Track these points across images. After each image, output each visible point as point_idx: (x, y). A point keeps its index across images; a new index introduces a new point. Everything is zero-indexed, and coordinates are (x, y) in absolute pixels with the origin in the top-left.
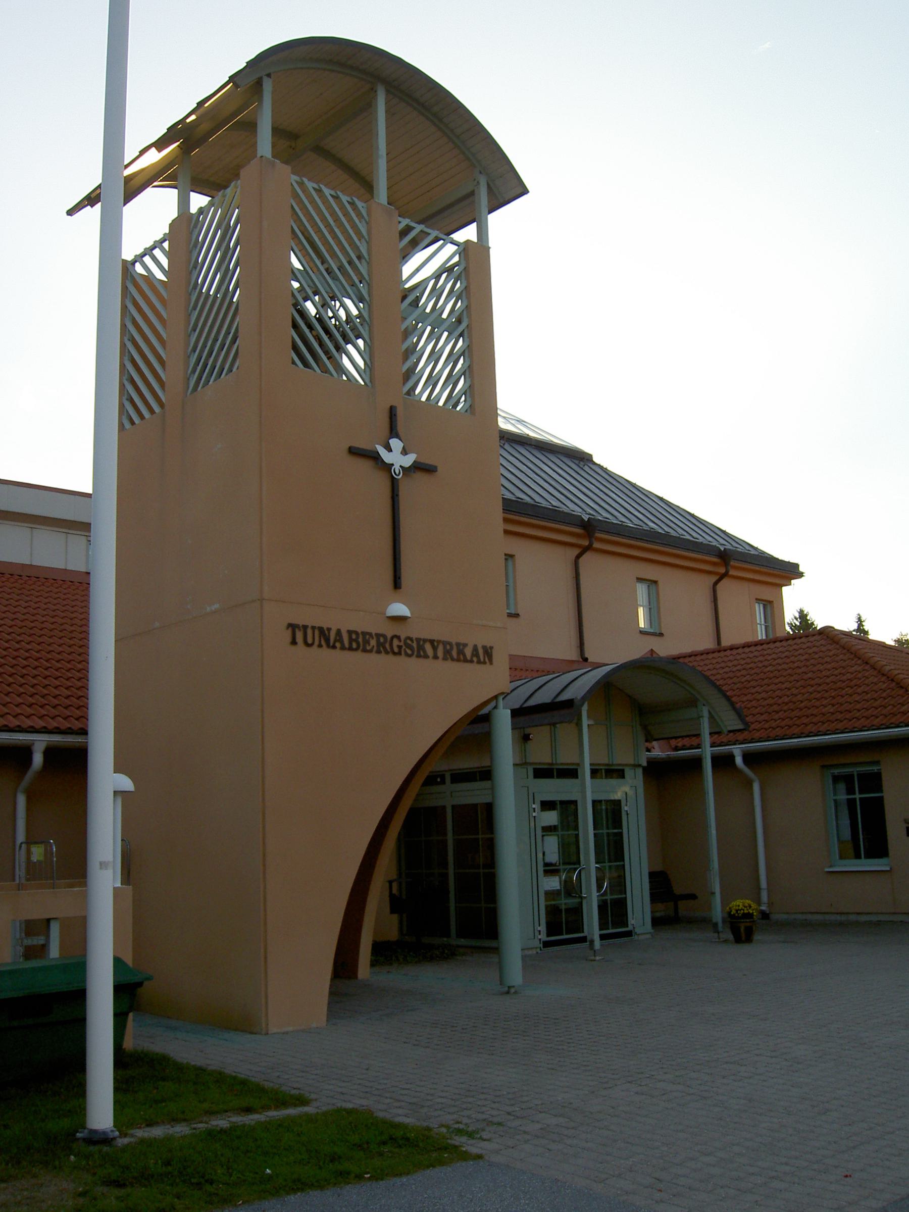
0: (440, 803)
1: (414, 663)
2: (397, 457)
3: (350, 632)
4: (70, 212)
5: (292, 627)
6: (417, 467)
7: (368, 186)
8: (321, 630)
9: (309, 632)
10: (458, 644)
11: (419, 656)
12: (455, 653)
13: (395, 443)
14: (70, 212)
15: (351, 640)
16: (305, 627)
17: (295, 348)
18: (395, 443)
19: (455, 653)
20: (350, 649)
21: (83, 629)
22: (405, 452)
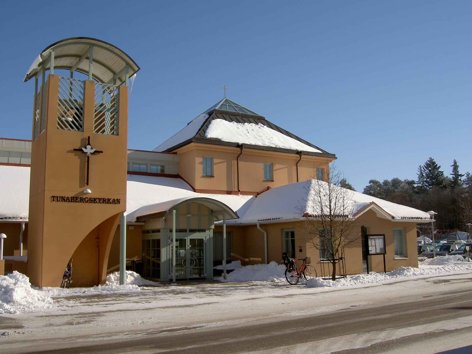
0: (149, 239)
1: (92, 205)
2: (89, 150)
3: (71, 197)
4: (102, 152)
5: (54, 197)
6: (96, 152)
7: (93, 75)
8: (62, 197)
9: (59, 198)
10: (108, 199)
11: (94, 202)
12: (106, 201)
13: (89, 147)
14: (102, 152)
15: (72, 199)
16: (57, 197)
17: (59, 124)
18: (89, 147)
19: (106, 201)
20: (72, 201)
21: (376, 260)
22: (92, 148)
